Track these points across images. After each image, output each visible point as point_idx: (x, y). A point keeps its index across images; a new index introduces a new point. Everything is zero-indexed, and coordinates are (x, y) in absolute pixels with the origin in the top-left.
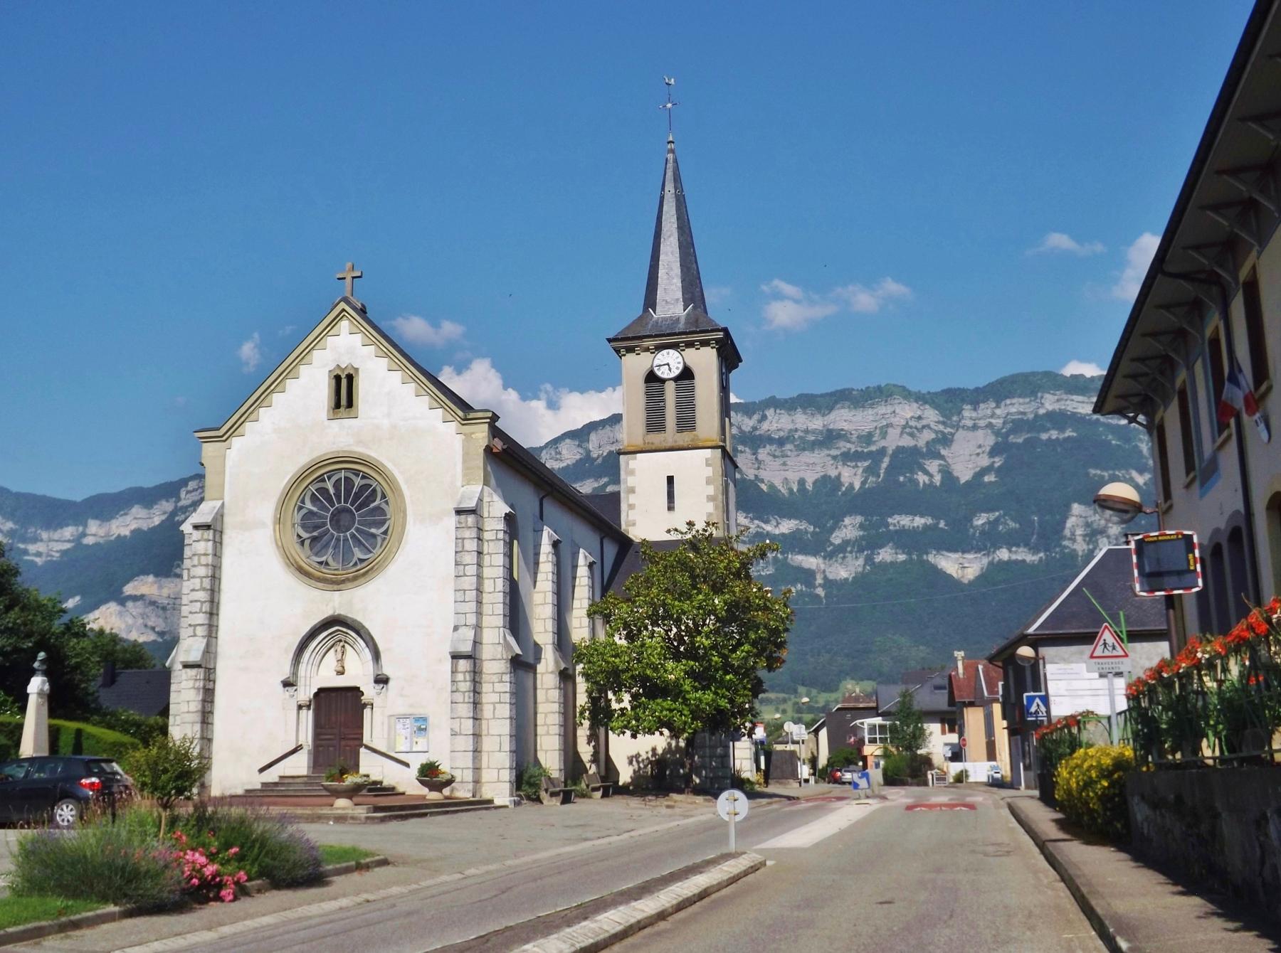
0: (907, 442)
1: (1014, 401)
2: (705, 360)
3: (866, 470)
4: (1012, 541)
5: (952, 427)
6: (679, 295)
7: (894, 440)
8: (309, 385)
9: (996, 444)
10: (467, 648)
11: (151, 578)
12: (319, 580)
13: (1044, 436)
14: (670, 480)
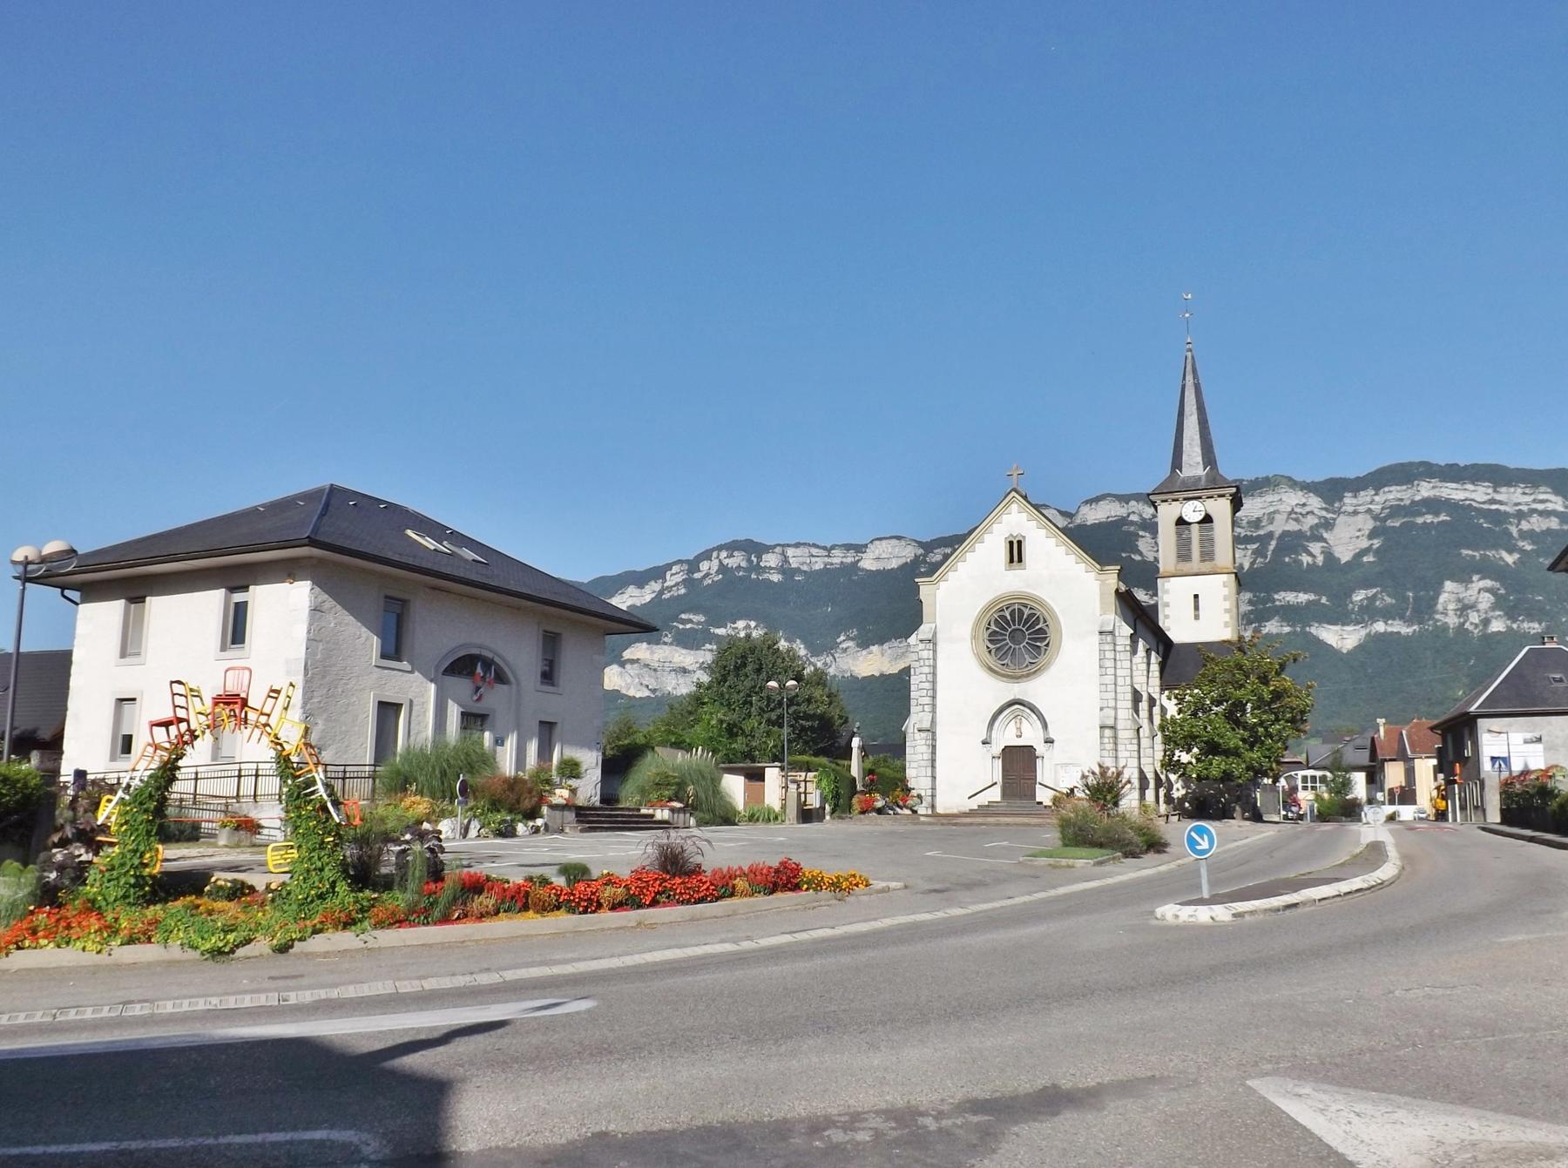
0: (1292, 526)
2: (1220, 508)
3: (1255, 552)
4: (1387, 615)
6: (1200, 459)
7: (1280, 526)
8: (987, 551)
10: (1110, 722)
11: (645, 645)
13: (1420, 520)
14: (1196, 596)
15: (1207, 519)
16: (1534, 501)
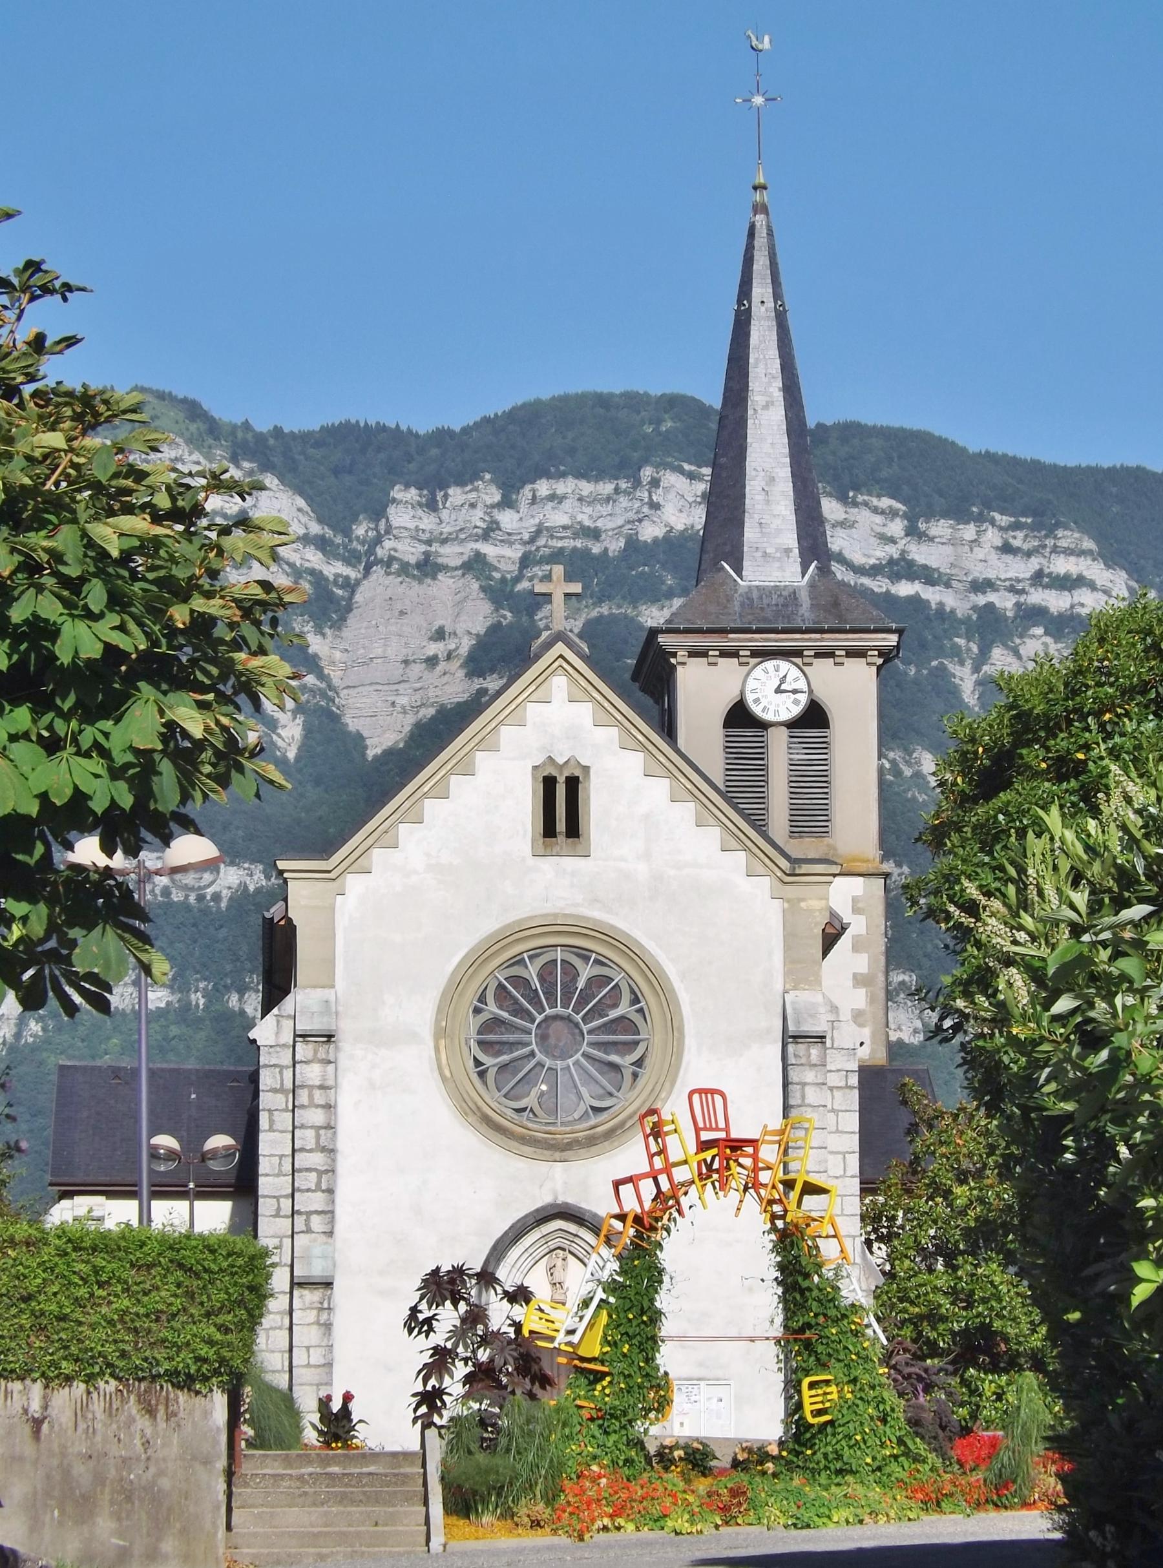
1: (566, 486)
5: (351, 559)
8: (484, 794)
9: (495, 629)
12: (523, 1140)
15: (814, 717)
16: (1038, 578)
